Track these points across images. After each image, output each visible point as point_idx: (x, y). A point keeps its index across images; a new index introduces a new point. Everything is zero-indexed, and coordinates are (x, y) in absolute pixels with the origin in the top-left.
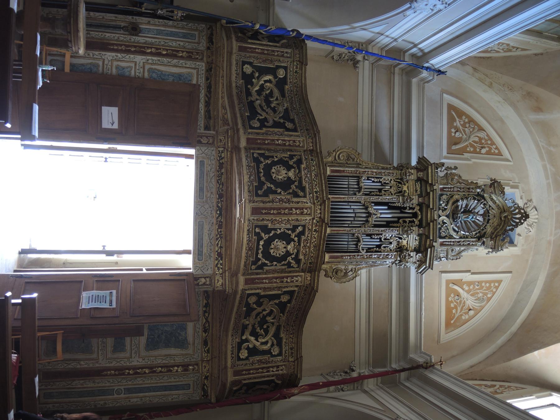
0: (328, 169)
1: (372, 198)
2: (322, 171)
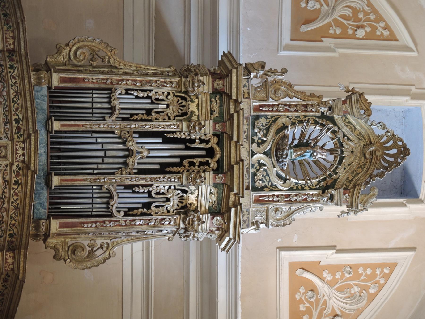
0: (55, 76)
1: (133, 126)
2: (27, 86)
